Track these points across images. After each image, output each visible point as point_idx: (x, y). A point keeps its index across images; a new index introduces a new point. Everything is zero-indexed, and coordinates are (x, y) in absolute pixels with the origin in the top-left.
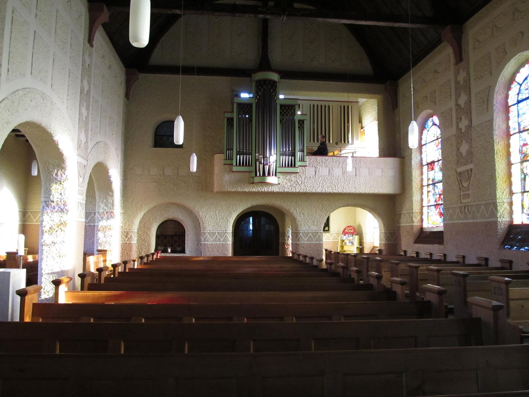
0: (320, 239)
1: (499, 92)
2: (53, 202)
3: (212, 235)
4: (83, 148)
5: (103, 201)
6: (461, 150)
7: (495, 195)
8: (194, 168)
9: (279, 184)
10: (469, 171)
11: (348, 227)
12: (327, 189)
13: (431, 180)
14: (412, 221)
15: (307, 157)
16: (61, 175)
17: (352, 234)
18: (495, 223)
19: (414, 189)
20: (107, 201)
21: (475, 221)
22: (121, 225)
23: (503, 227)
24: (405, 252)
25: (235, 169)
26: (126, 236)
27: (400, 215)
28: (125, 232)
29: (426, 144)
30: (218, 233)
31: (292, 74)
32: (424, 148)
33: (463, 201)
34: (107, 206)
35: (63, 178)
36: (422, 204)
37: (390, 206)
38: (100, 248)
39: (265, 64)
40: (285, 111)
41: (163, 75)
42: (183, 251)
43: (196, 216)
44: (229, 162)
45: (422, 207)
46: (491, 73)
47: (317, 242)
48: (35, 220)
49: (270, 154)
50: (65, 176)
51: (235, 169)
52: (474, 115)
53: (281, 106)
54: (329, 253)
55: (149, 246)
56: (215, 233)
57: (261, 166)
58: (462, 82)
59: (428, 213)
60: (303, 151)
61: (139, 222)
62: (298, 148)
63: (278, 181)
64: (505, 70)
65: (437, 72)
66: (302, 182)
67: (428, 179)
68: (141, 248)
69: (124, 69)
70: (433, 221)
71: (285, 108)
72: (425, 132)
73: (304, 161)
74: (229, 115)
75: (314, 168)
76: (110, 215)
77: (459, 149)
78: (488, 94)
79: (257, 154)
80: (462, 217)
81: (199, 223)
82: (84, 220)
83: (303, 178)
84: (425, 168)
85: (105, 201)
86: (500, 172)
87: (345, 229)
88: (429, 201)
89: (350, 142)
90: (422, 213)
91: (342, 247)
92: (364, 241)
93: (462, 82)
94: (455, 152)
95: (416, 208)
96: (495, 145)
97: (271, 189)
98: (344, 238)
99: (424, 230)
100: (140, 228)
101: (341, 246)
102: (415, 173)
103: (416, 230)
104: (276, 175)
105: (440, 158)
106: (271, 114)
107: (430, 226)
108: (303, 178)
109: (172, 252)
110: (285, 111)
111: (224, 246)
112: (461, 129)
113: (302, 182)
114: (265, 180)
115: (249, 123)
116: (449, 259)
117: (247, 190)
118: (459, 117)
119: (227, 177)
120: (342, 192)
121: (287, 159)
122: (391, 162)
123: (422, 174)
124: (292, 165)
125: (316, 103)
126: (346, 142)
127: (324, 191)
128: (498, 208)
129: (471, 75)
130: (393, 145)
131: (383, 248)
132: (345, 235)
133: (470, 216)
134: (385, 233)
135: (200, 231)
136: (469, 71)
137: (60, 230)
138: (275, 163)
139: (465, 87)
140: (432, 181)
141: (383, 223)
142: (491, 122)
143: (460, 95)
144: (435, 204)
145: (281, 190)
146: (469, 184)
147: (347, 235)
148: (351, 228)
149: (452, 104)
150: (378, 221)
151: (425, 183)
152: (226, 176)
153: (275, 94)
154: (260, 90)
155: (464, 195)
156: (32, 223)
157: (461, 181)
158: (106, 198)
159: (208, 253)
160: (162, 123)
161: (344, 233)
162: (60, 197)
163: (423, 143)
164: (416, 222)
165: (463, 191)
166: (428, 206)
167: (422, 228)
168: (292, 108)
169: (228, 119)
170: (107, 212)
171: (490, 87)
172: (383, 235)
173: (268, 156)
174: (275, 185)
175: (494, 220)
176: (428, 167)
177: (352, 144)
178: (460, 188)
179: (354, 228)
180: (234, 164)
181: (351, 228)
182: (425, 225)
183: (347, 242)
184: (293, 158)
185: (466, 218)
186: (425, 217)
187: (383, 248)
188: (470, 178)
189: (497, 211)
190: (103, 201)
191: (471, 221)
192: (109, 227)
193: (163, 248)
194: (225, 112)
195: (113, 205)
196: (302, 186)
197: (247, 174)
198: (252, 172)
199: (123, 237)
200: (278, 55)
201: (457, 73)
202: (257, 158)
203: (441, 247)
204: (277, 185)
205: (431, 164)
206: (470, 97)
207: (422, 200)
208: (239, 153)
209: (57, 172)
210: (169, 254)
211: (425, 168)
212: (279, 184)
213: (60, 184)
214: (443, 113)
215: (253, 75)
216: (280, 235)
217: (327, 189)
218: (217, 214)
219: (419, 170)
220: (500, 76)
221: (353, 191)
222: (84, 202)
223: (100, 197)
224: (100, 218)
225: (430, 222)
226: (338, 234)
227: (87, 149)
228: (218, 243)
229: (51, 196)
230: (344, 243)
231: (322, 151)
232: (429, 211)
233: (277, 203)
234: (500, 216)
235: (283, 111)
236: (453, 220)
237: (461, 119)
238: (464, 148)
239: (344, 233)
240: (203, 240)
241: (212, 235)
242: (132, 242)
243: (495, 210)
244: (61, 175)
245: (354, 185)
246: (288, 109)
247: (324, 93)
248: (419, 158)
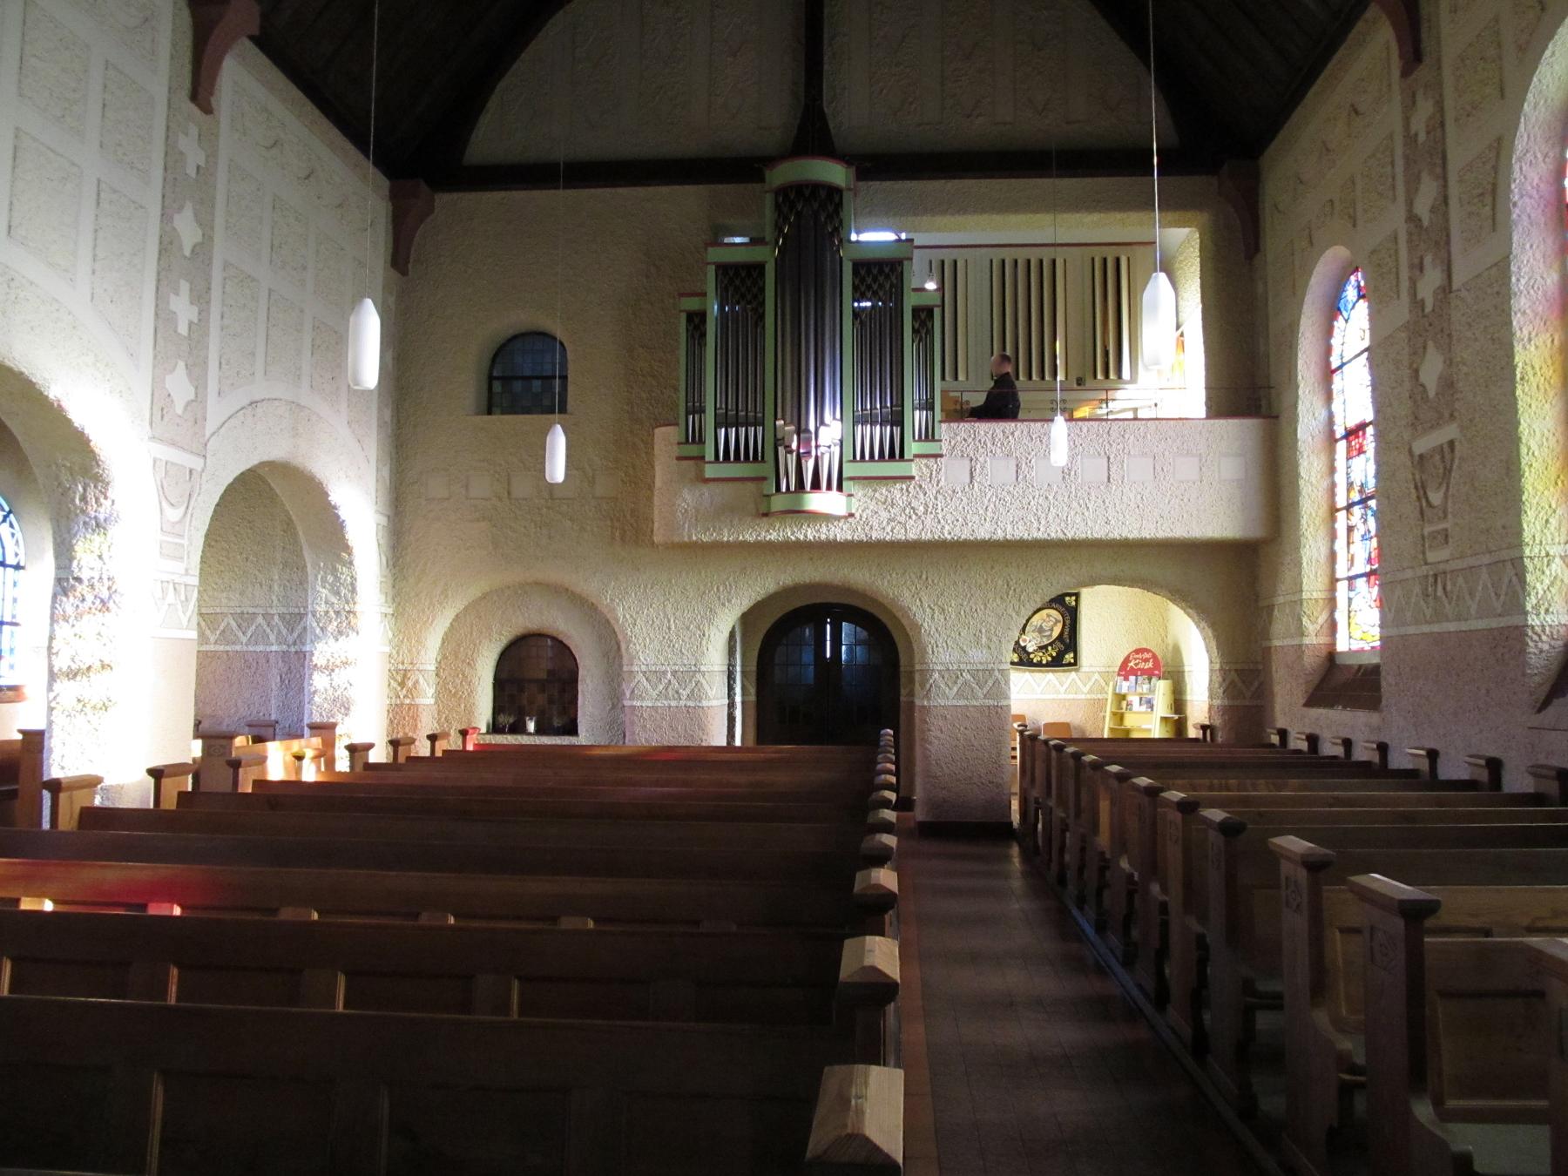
0: (999, 689)
1: (1529, 156)
2: (78, 580)
4: (180, 425)
5: (324, 580)
6: (1423, 378)
7: (1519, 532)
8: (557, 469)
9: (851, 515)
10: (1446, 449)
11: (1138, 651)
12: (1009, 527)
13: (1357, 488)
14: (1301, 632)
15: (944, 426)
16: (97, 500)
17: (1150, 674)
18: (1516, 636)
19: (1304, 522)
20: (337, 578)
21: (1464, 626)
22: (387, 649)
23: (1546, 647)
24: (1283, 734)
25: (710, 471)
26: (402, 684)
27: (1271, 608)
28: (398, 671)
29: (1343, 365)
30: (674, 673)
31: (898, 165)
32: (1337, 378)
33: (1432, 557)
34: (338, 593)
35: (102, 510)
36: (1333, 571)
37: (1237, 578)
38: (317, 719)
39: (812, 136)
40: (869, 280)
41: (503, 194)
42: (572, 730)
43: (608, 621)
44: (692, 450)
45: (1334, 581)
46: (1502, 90)
47: (991, 702)
49: (821, 421)
51: (710, 471)
52: (1456, 247)
53: (858, 266)
54: (1030, 741)
55: (470, 711)
56: (665, 673)
57: (792, 459)
58: (1422, 137)
59: (1350, 600)
60: (929, 406)
61: (439, 641)
62: (912, 394)
63: (849, 505)
64: (1543, 69)
65: (1357, 113)
66: (926, 506)
67: (1350, 486)
68: (447, 719)
69: (385, 183)
70: (1359, 628)
71: (869, 272)
72: (1339, 324)
73: (933, 440)
74: (692, 304)
75: (967, 462)
76: (346, 619)
77: (1417, 371)
78: (1495, 168)
79: (780, 423)
80: (1428, 612)
82: (194, 635)
83: (931, 493)
84: (1341, 447)
85: (330, 579)
86: (1534, 447)
87: (1127, 661)
88: (1352, 561)
89: (1126, 374)
90: (1332, 602)
91: (1119, 717)
92: (1189, 697)
93: (1422, 137)
94: (1407, 385)
95: (1313, 585)
96: (1518, 348)
97: (824, 533)
98: (1125, 687)
99: (1339, 661)
100: (445, 657)
101: (1114, 714)
102: (1310, 467)
103: (1311, 661)
104: (840, 488)
105: (1368, 415)
106: (823, 297)
107: (1355, 646)
108: (931, 493)
109: (540, 731)
110: (869, 280)
111: (695, 715)
112: (1422, 304)
113: (926, 506)
114: (800, 502)
115: (756, 325)
116: (1397, 761)
117: (750, 536)
118: (1416, 261)
119: (688, 498)
120: (1062, 536)
121: (876, 434)
122: (1236, 430)
123: (1332, 470)
124: (895, 453)
125: (1009, 255)
126: (1112, 376)
127: (1000, 535)
128: (1529, 578)
129: (1447, 107)
130: (1250, 380)
131: (1217, 722)
132: (1126, 679)
133: (1448, 609)
134: (1224, 672)
135: (621, 666)
136: (1441, 95)
138: (837, 450)
139: (1428, 155)
140: (1361, 492)
141: (1217, 638)
142: (1502, 268)
143: (1418, 179)
144: (1368, 569)
145: (860, 535)
146: (1446, 497)
147: (1132, 678)
148: (1146, 655)
149: (1396, 217)
150: (1202, 631)
151: (1341, 501)
152: (686, 494)
153: (836, 230)
154: (786, 219)
155: (1433, 535)
157: (1424, 488)
160: (515, 338)
161: (1125, 670)
162: (99, 563)
163: (1335, 363)
164: (1313, 636)
165: (1430, 522)
166: (1351, 579)
167: (1331, 656)
168: (893, 270)
169: (691, 316)
170: (337, 613)
171: (1499, 140)
172: (1218, 678)
173: (812, 427)
174: (838, 518)
175: (1515, 620)
176: (1349, 442)
177: (1133, 380)
178: (1422, 513)
179: (1154, 657)
180: (710, 456)
181: (1146, 655)
182: (1342, 645)
183: (1135, 699)
184: (897, 430)
185: (1439, 616)
186: (1341, 616)
187: (1217, 722)
188: (1448, 471)
189: (1524, 589)
190: (324, 580)
191: (1452, 627)
193: (511, 720)
194: (682, 295)
195: (353, 591)
196: (929, 520)
197: (751, 486)
198: (764, 479)
199: (394, 684)
200: (856, 107)
201: (1410, 104)
202: (779, 436)
203: (1374, 718)
204: (845, 518)
205: (1353, 433)
206: (1445, 186)
207: (1333, 556)
208: (723, 421)
210: (530, 737)
211: (1341, 447)
212: (851, 515)
214: (1373, 252)
215: (768, 174)
216: (903, 680)
217: (1009, 527)
219: (1323, 458)
220: (1530, 96)
221: (1099, 532)
222: (195, 581)
223: (316, 565)
224: (318, 631)
225: (1357, 634)
226: (1105, 675)
227: (199, 420)
228: (673, 703)
229: (75, 563)
230: (1124, 704)
231: (1000, 405)
232: (1352, 594)
233: (859, 576)
234: (1536, 607)
235: (863, 280)
236: (1404, 624)
237: (1421, 269)
238: (1432, 370)
239: (1125, 670)
242: (418, 701)
243: (1518, 588)
244: (97, 500)
245: (1103, 514)
246: (882, 274)
247: (1014, 219)
248: (1323, 414)
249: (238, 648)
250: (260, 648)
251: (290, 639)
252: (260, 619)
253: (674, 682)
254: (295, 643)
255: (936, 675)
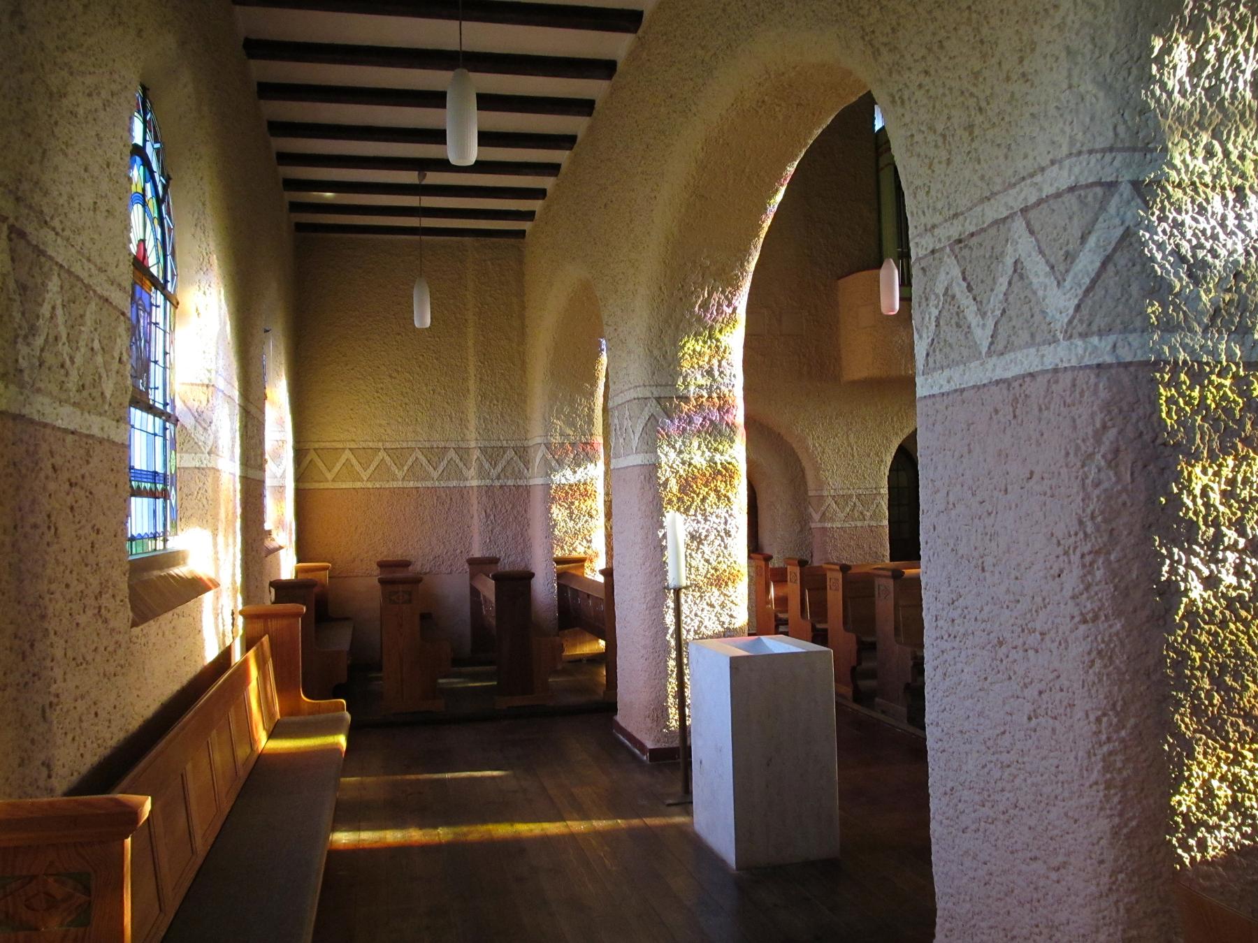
2: (686, 399)
3: (841, 502)
30: (858, 496)
34: (572, 425)
48: (330, 476)
50: (729, 311)
56: (851, 496)
81: (803, 471)
85: (566, 410)
135: (806, 491)
137: (712, 494)
156: (322, 486)
158: (572, 402)
159: (835, 554)
170: (573, 445)
192: (582, 488)
209: (710, 295)
213: (710, 337)
218: (852, 440)
228: (859, 524)
240: (816, 517)
241: (841, 502)
244: (720, 305)
249: (429, 484)
250: (454, 483)
251: (494, 473)
252: (452, 454)
253: (858, 504)
254: (498, 478)
255: (829, 501)
